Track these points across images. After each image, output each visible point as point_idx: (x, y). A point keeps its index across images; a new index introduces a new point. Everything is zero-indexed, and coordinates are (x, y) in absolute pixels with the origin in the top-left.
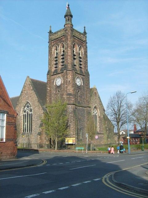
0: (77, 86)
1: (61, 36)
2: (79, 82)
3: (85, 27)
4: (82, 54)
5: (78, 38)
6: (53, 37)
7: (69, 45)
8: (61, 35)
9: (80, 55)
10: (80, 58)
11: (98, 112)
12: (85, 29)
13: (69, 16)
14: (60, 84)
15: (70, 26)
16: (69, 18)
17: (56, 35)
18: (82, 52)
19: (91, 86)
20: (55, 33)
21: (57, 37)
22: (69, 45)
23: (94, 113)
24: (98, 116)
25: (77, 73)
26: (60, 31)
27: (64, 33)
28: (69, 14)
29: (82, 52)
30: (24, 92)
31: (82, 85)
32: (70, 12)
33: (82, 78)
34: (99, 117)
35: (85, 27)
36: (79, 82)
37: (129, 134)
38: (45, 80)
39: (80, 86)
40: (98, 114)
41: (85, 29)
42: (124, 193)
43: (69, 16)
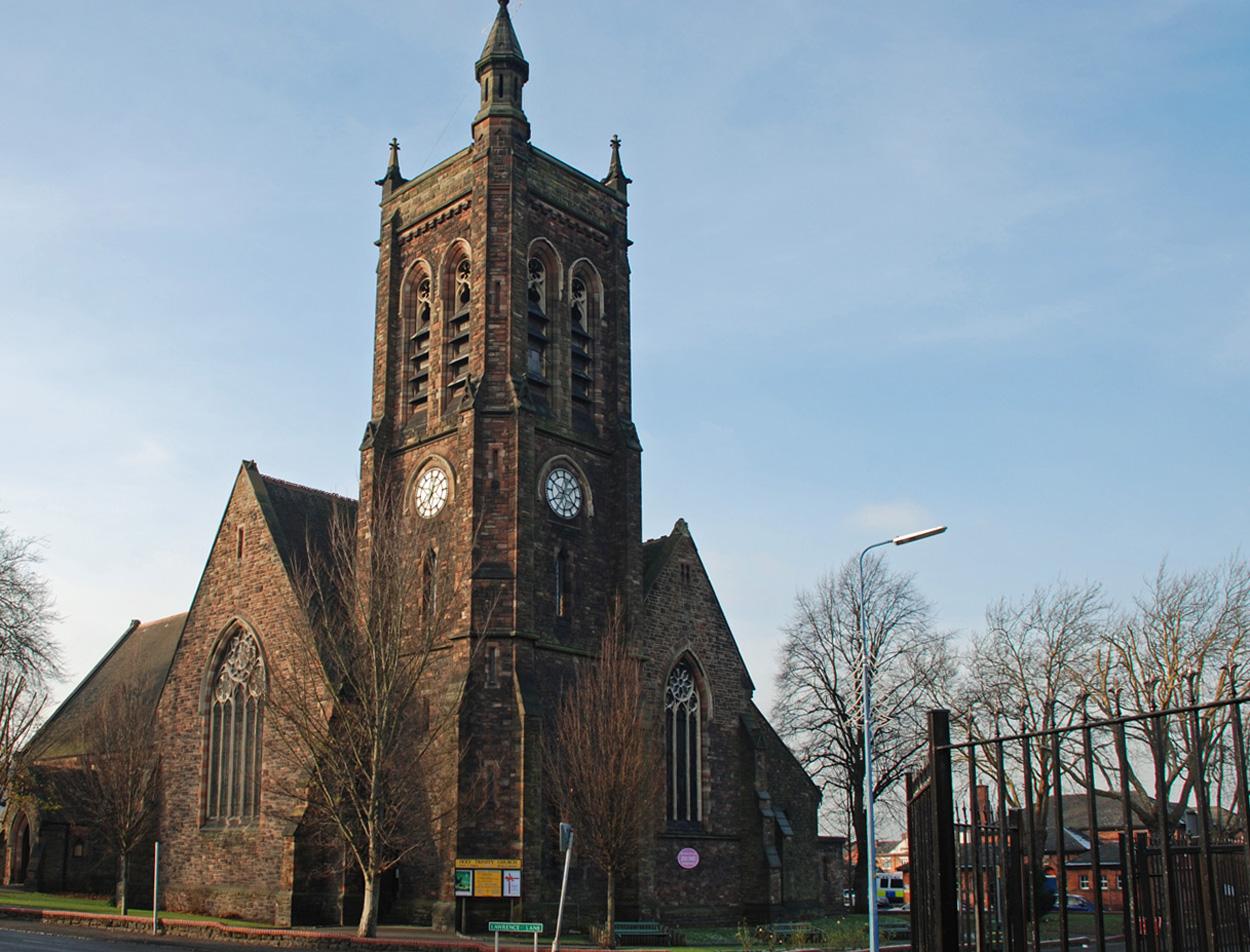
0: (553, 514)
1: (449, 199)
2: (563, 493)
3: (616, 144)
4: (593, 314)
5: (565, 210)
6: (409, 208)
7: (525, 288)
8: (454, 189)
9: (584, 323)
10: (582, 338)
11: (703, 695)
12: (616, 157)
13: (506, 67)
14: (441, 504)
15: (507, 128)
16: (507, 80)
17: (425, 195)
18: (592, 302)
19: (654, 527)
20: (420, 184)
21: (428, 207)
22: (525, 288)
23: (670, 697)
24: (703, 718)
25: (551, 435)
26: (446, 168)
27: (467, 179)
28: (503, 53)
29: (592, 302)
30: (223, 565)
31: (591, 509)
32: (513, 44)
33: (590, 469)
34: (712, 729)
35: (616, 144)
36: (563, 493)
37: (152, 909)
38: (357, 499)
39: (573, 520)
40: (703, 710)
41: (616, 157)
42: (688, 775)
43: (506, 67)
